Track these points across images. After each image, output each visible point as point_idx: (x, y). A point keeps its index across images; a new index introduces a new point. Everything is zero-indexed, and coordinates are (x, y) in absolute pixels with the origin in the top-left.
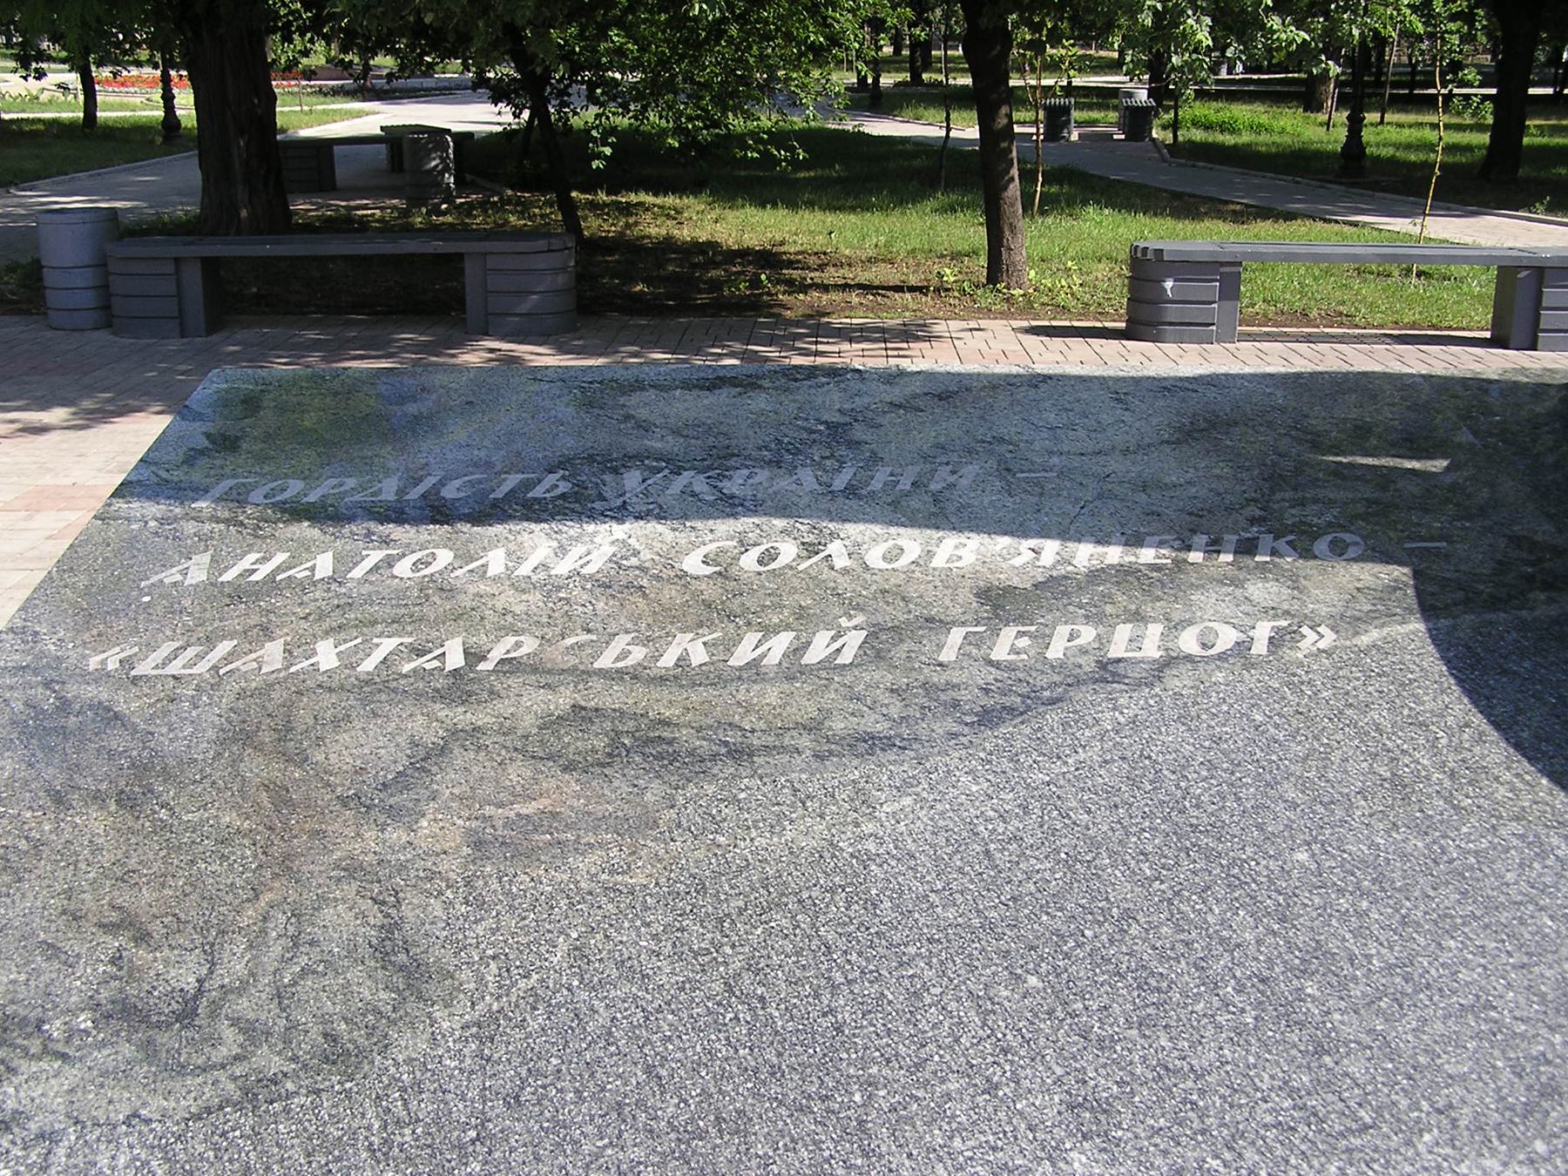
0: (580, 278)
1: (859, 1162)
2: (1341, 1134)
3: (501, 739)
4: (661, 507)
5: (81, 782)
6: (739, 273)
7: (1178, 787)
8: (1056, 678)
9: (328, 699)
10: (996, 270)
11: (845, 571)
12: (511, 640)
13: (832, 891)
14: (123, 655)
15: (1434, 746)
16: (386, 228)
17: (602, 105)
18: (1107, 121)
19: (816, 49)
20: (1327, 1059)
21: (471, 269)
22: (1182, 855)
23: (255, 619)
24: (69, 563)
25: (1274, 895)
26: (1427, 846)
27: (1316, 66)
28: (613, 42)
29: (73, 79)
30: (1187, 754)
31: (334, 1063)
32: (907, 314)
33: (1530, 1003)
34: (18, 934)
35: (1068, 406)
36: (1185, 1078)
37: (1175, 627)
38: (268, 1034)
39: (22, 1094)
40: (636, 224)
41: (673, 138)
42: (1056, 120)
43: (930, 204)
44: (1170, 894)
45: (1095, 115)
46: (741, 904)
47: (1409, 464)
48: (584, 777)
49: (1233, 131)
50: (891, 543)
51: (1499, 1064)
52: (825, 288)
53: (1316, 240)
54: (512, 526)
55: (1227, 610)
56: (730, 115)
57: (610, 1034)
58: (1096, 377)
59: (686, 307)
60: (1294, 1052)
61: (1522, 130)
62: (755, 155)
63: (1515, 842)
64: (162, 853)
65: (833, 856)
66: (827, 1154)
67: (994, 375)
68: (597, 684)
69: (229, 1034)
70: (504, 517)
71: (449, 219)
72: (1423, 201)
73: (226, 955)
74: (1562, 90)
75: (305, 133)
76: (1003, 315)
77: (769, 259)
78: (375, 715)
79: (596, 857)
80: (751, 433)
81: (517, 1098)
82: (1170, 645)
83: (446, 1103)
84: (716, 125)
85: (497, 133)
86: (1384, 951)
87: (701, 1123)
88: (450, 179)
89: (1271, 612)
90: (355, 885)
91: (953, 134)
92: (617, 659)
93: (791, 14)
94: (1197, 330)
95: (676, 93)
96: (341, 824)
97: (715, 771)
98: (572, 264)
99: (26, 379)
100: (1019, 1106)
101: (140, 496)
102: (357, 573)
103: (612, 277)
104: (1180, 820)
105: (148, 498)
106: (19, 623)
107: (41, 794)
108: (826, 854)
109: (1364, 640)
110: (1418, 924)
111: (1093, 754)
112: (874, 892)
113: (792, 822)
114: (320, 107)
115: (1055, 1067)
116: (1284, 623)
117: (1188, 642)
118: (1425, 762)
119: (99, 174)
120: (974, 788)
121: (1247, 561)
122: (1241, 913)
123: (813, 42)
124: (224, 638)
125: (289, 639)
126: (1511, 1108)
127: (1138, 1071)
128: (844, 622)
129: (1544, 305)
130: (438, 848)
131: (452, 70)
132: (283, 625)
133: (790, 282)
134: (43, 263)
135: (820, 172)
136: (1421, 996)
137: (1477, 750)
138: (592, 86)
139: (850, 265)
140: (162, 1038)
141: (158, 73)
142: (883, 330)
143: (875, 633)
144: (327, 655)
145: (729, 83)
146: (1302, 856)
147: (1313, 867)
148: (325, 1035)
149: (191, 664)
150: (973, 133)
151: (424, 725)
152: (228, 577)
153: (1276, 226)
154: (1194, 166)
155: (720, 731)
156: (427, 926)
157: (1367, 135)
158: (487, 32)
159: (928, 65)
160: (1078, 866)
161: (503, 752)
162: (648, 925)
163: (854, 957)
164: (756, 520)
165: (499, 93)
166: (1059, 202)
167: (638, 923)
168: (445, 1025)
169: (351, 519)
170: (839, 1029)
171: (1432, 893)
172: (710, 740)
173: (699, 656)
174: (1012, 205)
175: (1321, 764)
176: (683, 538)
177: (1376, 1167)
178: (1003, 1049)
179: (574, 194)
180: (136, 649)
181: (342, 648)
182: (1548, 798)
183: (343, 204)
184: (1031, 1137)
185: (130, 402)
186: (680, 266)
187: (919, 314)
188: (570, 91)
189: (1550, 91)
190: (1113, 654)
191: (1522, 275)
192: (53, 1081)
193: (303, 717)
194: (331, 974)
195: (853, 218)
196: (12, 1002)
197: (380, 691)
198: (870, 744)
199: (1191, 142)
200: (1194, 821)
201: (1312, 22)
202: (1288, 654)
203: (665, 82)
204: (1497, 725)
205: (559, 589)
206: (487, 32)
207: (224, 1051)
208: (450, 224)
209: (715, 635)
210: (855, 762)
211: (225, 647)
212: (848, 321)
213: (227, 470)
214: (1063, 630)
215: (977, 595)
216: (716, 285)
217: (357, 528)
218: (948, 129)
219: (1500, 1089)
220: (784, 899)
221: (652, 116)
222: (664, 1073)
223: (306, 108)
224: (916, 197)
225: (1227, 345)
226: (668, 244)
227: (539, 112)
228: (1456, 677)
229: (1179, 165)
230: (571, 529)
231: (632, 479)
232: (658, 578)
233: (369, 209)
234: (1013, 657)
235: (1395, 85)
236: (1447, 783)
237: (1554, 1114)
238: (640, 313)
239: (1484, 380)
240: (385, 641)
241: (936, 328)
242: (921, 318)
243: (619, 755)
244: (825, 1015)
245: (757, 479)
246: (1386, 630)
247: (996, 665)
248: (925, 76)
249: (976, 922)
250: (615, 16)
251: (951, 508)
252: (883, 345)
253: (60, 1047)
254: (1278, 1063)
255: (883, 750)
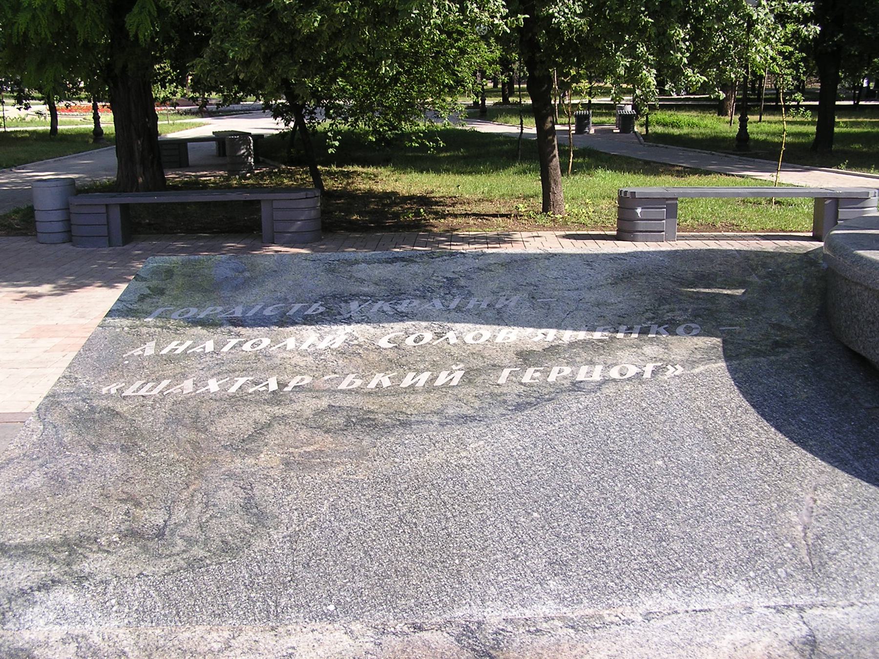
0: (323, 212)
1: (457, 586)
2: (667, 572)
3: (296, 420)
4: (368, 318)
5: (104, 441)
6: (409, 208)
7: (605, 435)
8: (552, 390)
9: (215, 405)
10: (547, 205)
11: (455, 345)
12: (299, 378)
13: (447, 480)
14: (117, 387)
15: (724, 416)
16: (217, 187)
17: (333, 119)
18: (610, 122)
19: (450, 87)
20: (664, 543)
21: (265, 209)
22: (605, 463)
23: (178, 370)
24: (88, 346)
25: (645, 478)
26: (716, 457)
27: (713, 94)
28: (339, 85)
29: (44, 108)
30: (610, 421)
31: (227, 552)
32: (500, 229)
33: (755, 519)
34: (82, 504)
35: (563, 268)
36: (601, 552)
37: (608, 367)
38: (197, 541)
39: (91, 566)
40: (353, 183)
41: (372, 135)
42: (582, 122)
43: (512, 170)
44: (599, 479)
45: (604, 119)
46: (406, 486)
47: (725, 292)
48: (335, 435)
49: (679, 127)
50: (476, 332)
51: (739, 543)
52: (455, 216)
53: (721, 185)
54: (297, 327)
55: (633, 359)
56: (403, 123)
57: (348, 539)
58: (578, 254)
59: (381, 227)
60: (649, 541)
61: (834, 124)
62: (417, 145)
63: (756, 455)
64: (144, 470)
65: (448, 466)
66: (443, 583)
67: (528, 254)
68: (340, 396)
69: (179, 542)
70: (294, 323)
71: (251, 181)
72: (777, 163)
73: (176, 511)
74: (858, 102)
75: (171, 136)
76: (551, 229)
77: (425, 201)
78: (238, 411)
79: (341, 468)
80: (411, 283)
81: (308, 564)
82: (605, 375)
83: (277, 567)
84: (395, 128)
85: (276, 134)
86: (693, 500)
87: (389, 573)
88: (251, 160)
89: (654, 359)
90: (232, 482)
91: (525, 131)
92: (349, 385)
93: (435, 68)
94: (654, 234)
95: (373, 112)
96: (225, 457)
97: (394, 432)
98: (319, 205)
99: (28, 269)
100: (527, 564)
101: (119, 316)
102: (226, 349)
103: (340, 212)
104: (606, 448)
105: (123, 317)
106: (68, 374)
107: (86, 446)
108: (445, 466)
109: (696, 371)
110: (709, 489)
111: (567, 422)
112: (465, 480)
113: (429, 452)
114: (179, 121)
115: (544, 548)
116: (660, 364)
117: (614, 373)
118: (720, 422)
119: (60, 160)
120: (512, 437)
121: (645, 337)
122: (630, 486)
123: (447, 84)
124: (165, 379)
125: (195, 379)
126: (742, 560)
127: (580, 549)
128: (454, 367)
129: (839, 218)
130: (269, 466)
131: (250, 101)
132: (192, 372)
133: (436, 213)
134: (35, 208)
135: (452, 153)
136: (708, 518)
137: (744, 417)
138: (328, 109)
139: (469, 203)
140: (150, 544)
141: (91, 104)
142: (486, 238)
143: (468, 372)
144: (213, 385)
145: (402, 106)
146: (660, 463)
147: (664, 467)
148: (222, 542)
149: (150, 390)
150: (534, 131)
151: (261, 415)
152: (164, 352)
153: (700, 178)
154: (657, 146)
155: (396, 415)
156: (266, 498)
157: (749, 128)
158: (273, 83)
159: (512, 94)
160: (558, 468)
161: (297, 425)
162: (364, 495)
163: (456, 506)
164: (413, 323)
165: (277, 113)
166: (582, 167)
167: (360, 495)
168: (275, 537)
169: (221, 325)
170: (449, 535)
171: (717, 477)
172: (392, 419)
173: (386, 383)
174: (555, 169)
175: (671, 424)
176: (378, 331)
177: (681, 584)
178: (521, 542)
179: (319, 167)
180: (124, 384)
181: (220, 382)
182: (774, 437)
183: (193, 174)
184: (532, 575)
185: (83, 281)
186: (377, 205)
187: (505, 229)
188: (315, 111)
189: (851, 103)
190: (579, 379)
191: (828, 202)
192: (104, 561)
193: (204, 412)
194: (223, 518)
195: (470, 178)
196: (83, 531)
197: (239, 400)
198: (465, 419)
199: (655, 133)
200: (612, 449)
201: (710, 71)
202: (660, 377)
203: (367, 107)
204: (754, 406)
205: (321, 355)
206: (273, 83)
207: (178, 548)
208: (252, 184)
209: (394, 374)
210: (458, 427)
211: (165, 383)
212: (468, 233)
213: (160, 304)
214: (556, 369)
215: (516, 354)
216: (396, 215)
217: (225, 329)
218: (522, 130)
219: (738, 553)
220: (425, 484)
221: (361, 124)
222: (372, 553)
223: (171, 122)
224: (504, 166)
225: (671, 243)
226: (370, 194)
227: (299, 123)
228: (738, 386)
229: (649, 146)
230: (326, 328)
231: (354, 305)
232: (367, 349)
233: (208, 177)
234: (532, 381)
235: (766, 100)
236: (729, 431)
237: (759, 562)
238: (355, 230)
239: (766, 252)
240: (297, 305)
241: (515, 236)
242: (507, 231)
243: (350, 426)
244: (443, 529)
245: (414, 304)
246: (707, 366)
247: (524, 385)
248: (510, 99)
249: (511, 492)
250: (340, 71)
251: (505, 316)
252: (486, 246)
253: (106, 548)
254: (642, 545)
255: (471, 421)
